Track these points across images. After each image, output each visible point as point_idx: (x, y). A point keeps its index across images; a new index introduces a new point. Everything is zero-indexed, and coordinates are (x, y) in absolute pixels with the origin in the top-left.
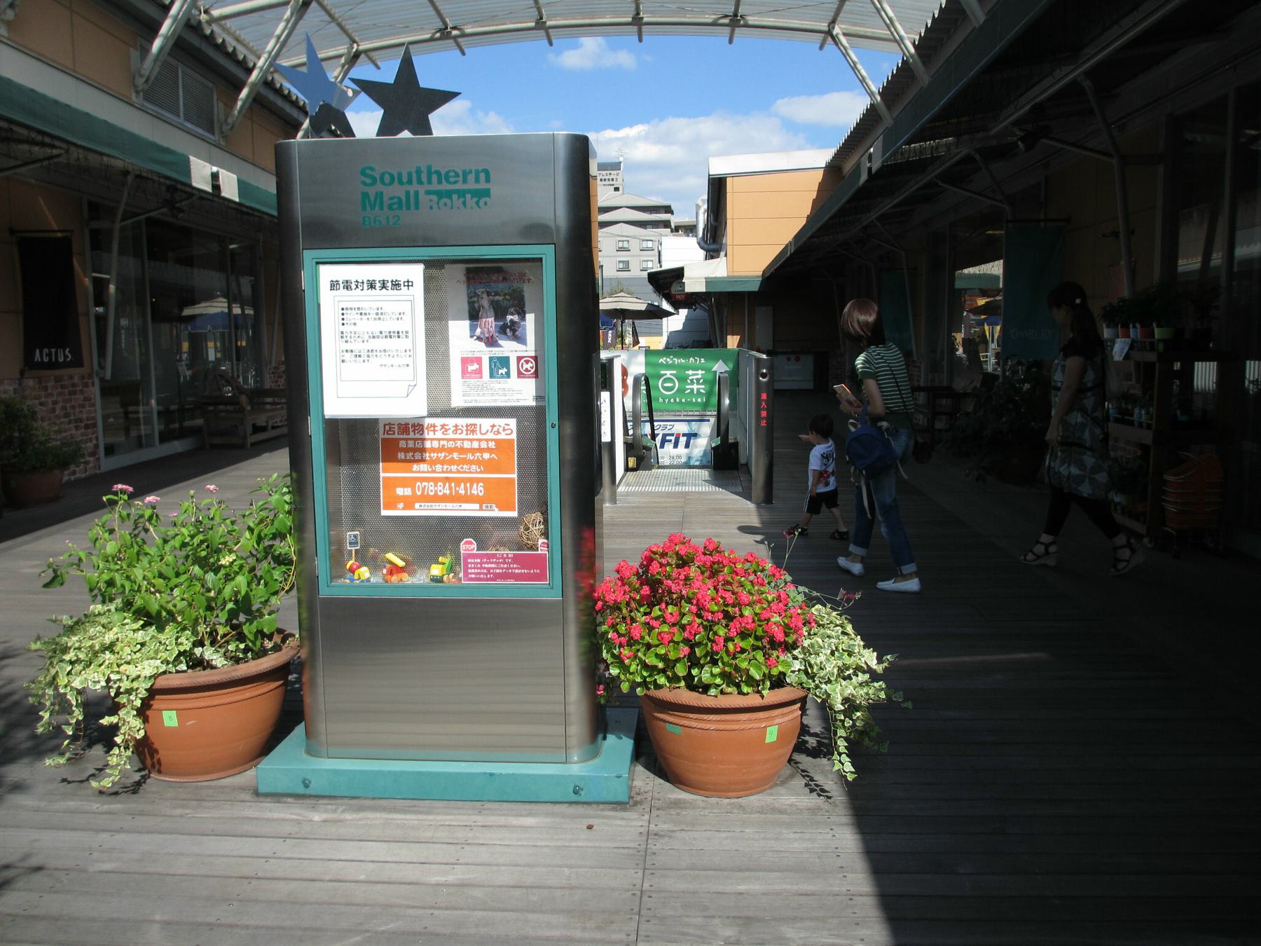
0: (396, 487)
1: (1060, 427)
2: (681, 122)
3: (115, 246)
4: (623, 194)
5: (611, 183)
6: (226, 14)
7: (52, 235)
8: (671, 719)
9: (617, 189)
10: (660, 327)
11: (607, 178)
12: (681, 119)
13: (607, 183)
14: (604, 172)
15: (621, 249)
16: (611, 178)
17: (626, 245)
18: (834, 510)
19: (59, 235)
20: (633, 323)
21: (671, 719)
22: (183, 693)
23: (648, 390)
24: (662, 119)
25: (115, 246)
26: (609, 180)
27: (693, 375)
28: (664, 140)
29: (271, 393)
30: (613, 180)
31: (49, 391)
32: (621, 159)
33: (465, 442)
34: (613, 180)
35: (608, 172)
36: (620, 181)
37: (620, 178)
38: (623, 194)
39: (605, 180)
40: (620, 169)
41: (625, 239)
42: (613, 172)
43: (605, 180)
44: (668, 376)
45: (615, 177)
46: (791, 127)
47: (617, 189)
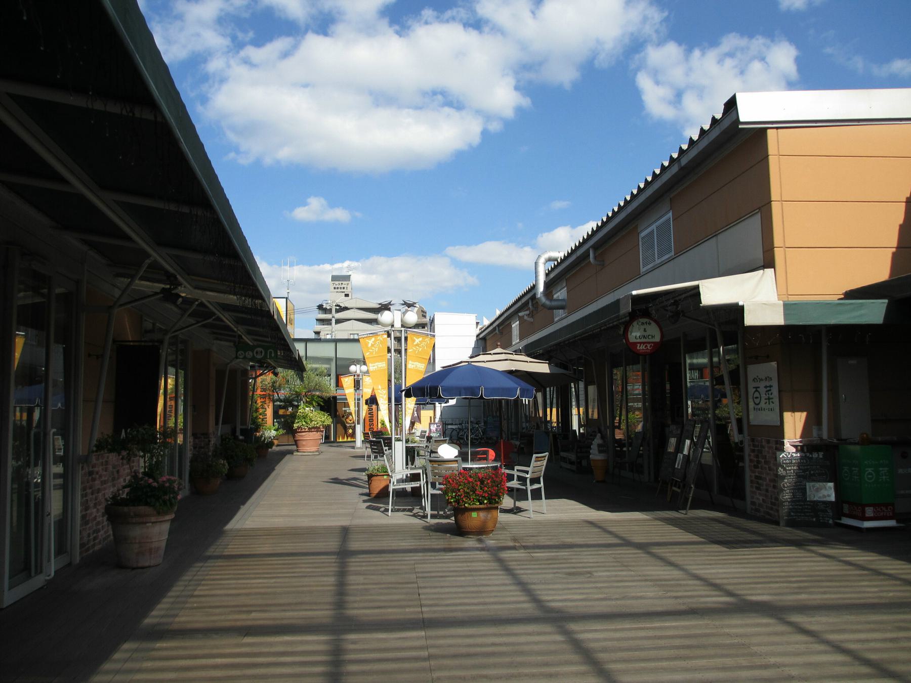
0: (349, 366)
1: (680, 511)
2: (382, 259)
4: (352, 299)
5: (342, 290)
7: (128, 343)
8: (353, 560)
9: (347, 295)
11: (339, 286)
12: (382, 257)
13: (339, 290)
14: (337, 283)
18: (130, 335)
19: (132, 344)
21: (353, 560)
24: (368, 258)
26: (341, 288)
27: (883, 470)
29: (786, 472)
30: (344, 288)
31: (772, 484)
33: (355, 335)
35: (340, 282)
36: (349, 289)
37: (349, 287)
38: (352, 299)
39: (338, 288)
42: (344, 282)
43: (338, 288)
44: (870, 471)
45: (345, 286)
46: (457, 264)
47: (347, 295)
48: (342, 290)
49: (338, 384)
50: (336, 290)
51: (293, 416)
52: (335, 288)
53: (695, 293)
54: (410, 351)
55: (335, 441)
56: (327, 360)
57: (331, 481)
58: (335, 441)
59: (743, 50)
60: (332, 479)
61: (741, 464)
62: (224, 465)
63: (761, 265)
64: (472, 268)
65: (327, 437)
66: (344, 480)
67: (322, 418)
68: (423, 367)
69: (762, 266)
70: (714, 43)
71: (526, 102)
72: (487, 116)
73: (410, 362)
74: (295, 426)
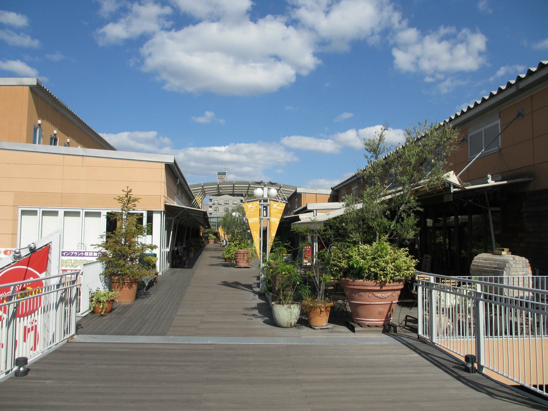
3: (502, 276)
5: (222, 179)
6: (451, 355)
10: (429, 272)
13: (221, 179)
14: (220, 176)
15: (226, 204)
16: (222, 178)
17: (228, 202)
20: (524, 286)
22: (484, 109)
23: (123, 309)
25: (502, 276)
28: (237, 152)
30: (223, 178)
32: (226, 171)
34: (223, 178)
35: (222, 176)
39: (220, 178)
40: (226, 175)
41: (227, 200)
42: (223, 176)
43: (220, 178)
45: (224, 177)
46: (288, 149)
48: (222, 179)
49: (218, 229)
50: (220, 179)
51: (208, 236)
52: (219, 178)
53: (33, 278)
54: (247, 213)
55: (217, 243)
56: (215, 222)
57: (222, 283)
58: (217, 243)
59: (454, 36)
60: (223, 282)
61: (474, 326)
62: (490, 176)
63: (500, 180)
64: (298, 152)
65: (215, 242)
66: (230, 283)
67: (214, 237)
68: (258, 219)
69: (500, 180)
70: (436, 29)
71: (319, 62)
72: (298, 67)
73: (249, 219)
74: (209, 238)
